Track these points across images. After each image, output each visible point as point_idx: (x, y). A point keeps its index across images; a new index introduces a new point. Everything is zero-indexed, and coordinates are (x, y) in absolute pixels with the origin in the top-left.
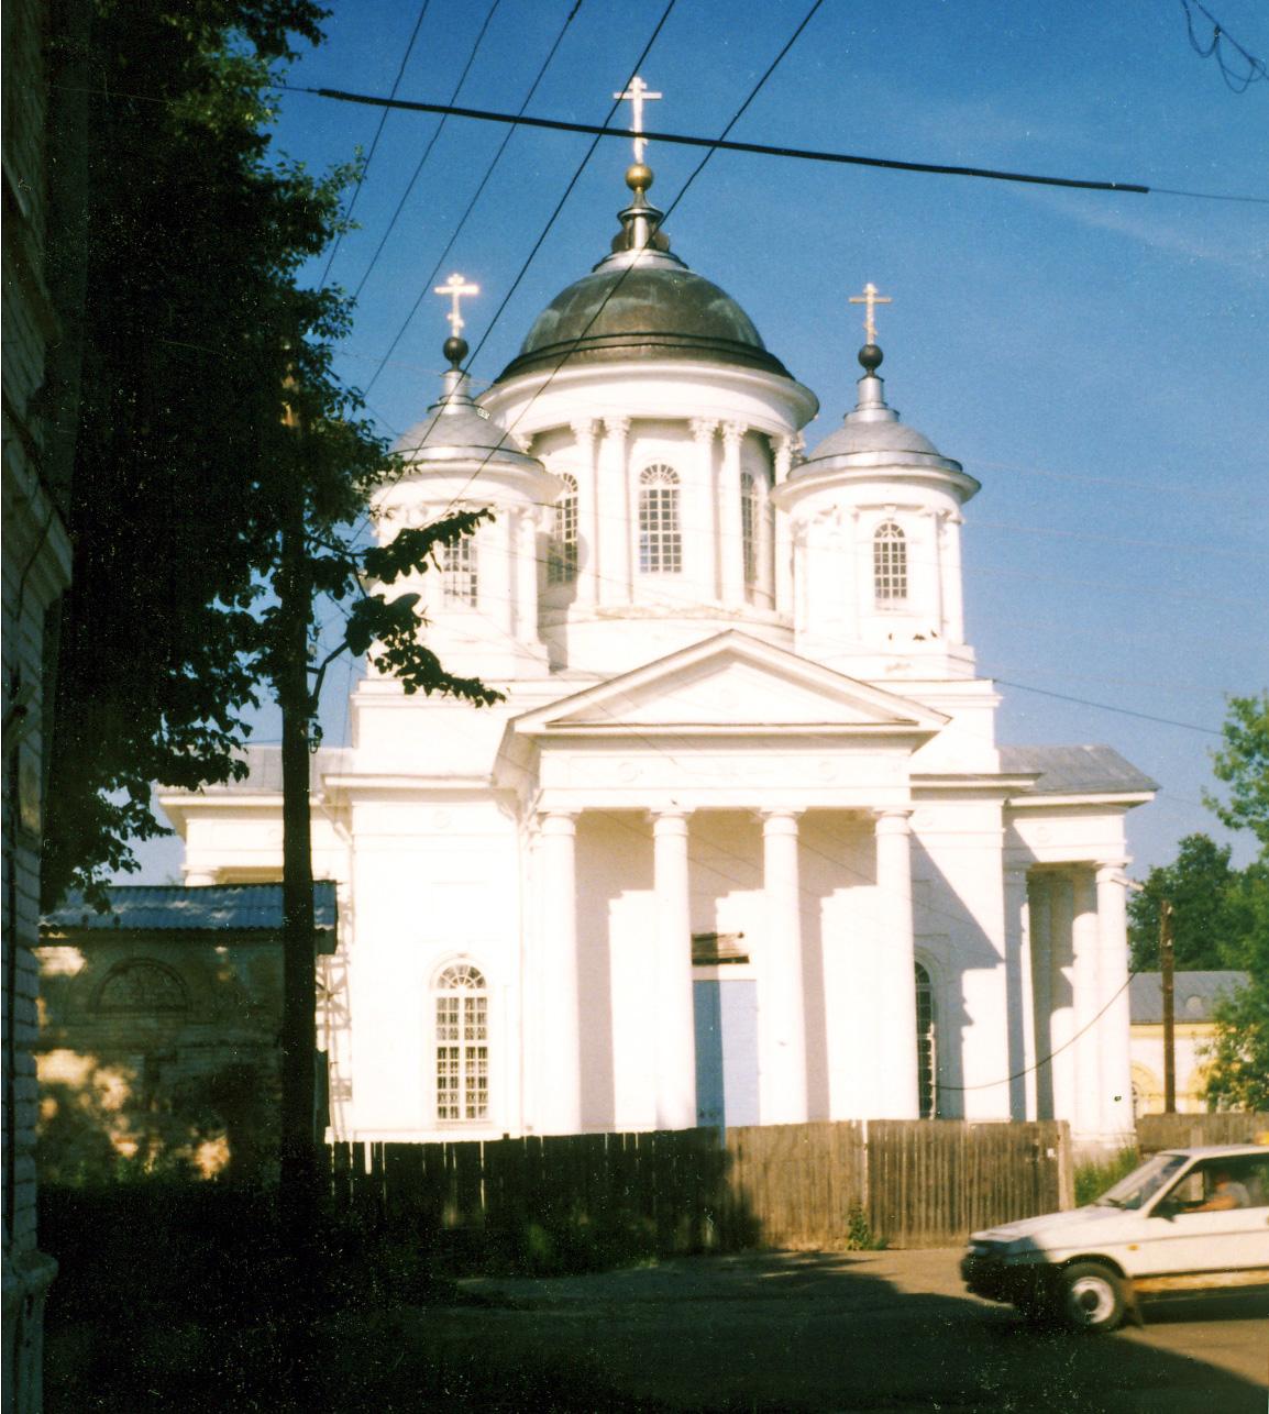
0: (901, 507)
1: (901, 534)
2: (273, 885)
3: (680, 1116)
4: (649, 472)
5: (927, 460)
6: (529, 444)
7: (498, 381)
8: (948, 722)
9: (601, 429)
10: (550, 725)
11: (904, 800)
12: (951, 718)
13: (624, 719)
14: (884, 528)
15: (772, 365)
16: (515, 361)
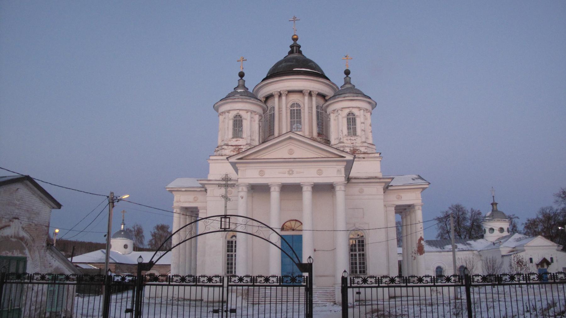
0: (353, 107)
1: (354, 115)
4: (293, 105)
5: (360, 95)
9: (280, 95)
14: (237, 116)
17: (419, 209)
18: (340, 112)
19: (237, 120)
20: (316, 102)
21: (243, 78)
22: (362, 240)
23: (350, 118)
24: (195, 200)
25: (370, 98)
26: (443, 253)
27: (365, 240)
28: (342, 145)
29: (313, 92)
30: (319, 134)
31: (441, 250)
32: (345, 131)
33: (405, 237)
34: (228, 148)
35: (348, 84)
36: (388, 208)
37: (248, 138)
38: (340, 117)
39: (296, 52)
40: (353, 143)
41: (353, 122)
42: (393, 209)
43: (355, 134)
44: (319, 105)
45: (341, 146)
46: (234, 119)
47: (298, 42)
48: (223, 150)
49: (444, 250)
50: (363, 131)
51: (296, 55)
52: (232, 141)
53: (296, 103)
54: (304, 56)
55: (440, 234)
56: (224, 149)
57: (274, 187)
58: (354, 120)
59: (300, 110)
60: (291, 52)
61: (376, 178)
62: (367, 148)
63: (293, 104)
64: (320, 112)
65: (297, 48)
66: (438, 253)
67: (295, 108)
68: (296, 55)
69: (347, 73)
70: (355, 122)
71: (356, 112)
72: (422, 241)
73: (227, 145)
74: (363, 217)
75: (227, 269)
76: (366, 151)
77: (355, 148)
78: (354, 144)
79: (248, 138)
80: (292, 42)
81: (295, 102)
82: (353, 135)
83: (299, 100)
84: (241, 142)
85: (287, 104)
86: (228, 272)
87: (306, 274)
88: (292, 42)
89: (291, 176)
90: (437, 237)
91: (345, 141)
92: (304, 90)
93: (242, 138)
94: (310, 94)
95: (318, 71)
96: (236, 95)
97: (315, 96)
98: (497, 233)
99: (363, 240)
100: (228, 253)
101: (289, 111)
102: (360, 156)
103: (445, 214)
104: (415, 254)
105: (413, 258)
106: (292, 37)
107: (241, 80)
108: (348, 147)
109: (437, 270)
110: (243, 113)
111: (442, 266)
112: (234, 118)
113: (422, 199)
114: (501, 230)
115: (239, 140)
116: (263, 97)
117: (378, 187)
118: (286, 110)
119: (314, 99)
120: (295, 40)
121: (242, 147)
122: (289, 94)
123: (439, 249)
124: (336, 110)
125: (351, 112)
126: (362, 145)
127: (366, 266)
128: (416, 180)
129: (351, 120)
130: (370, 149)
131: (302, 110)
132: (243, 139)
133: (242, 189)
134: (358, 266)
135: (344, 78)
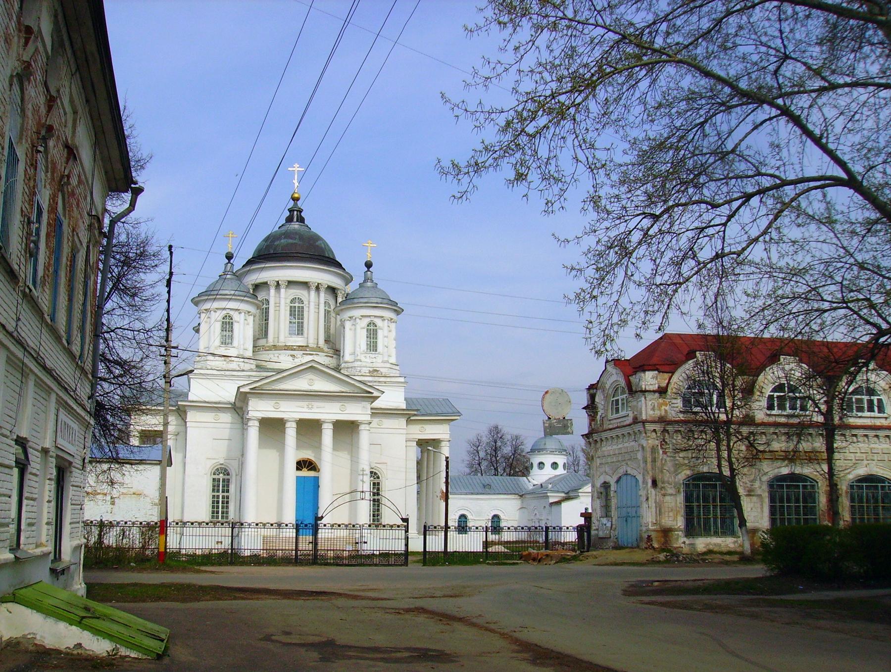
0: (375, 316)
1: (376, 326)
3: (441, 548)
4: (293, 301)
5: (385, 301)
9: (278, 285)
10: (251, 389)
11: (367, 418)
13: (278, 388)
14: (226, 316)
28: (359, 363)
30: (327, 341)
32: (364, 346)
38: (358, 327)
39: (297, 221)
58: (375, 332)
59: (303, 307)
60: (289, 220)
67: (297, 305)
68: (295, 226)
69: (369, 265)
89: (310, 411)
91: (363, 359)
94: (318, 288)
98: (548, 470)
100: (214, 494)
114: (555, 465)
119: (322, 294)
129: (372, 333)
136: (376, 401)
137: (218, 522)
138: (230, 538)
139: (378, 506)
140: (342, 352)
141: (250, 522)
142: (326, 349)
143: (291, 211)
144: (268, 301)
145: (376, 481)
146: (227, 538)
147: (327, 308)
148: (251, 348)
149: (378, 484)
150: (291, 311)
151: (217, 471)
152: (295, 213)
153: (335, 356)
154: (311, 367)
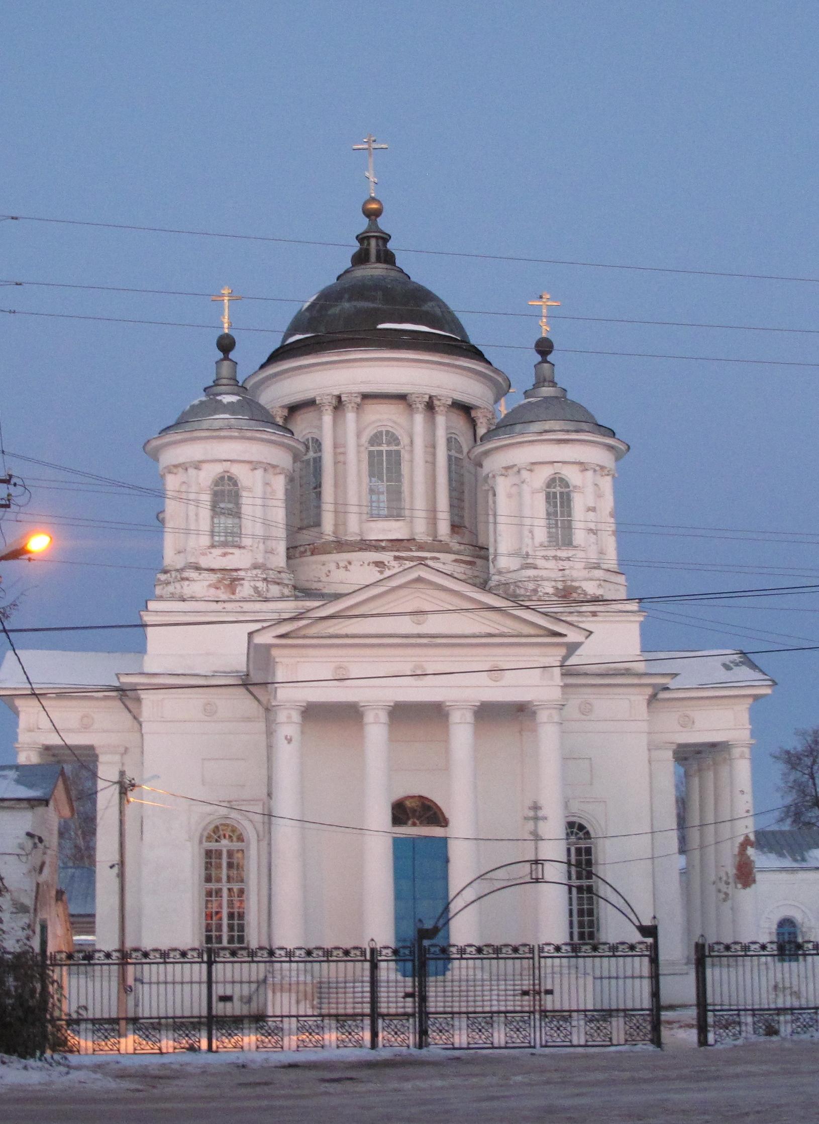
1: (567, 486)
2: (126, 1011)
4: (375, 439)
5: (584, 426)
6: (286, 412)
7: (263, 366)
8: (589, 635)
12: (591, 632)
14: (222, 478)
15: (476, 354)
16: (277, 350)
17: (742, 757)
18: (525, 474)
19: (223, 491)
20: (448, 428)
21: (232, 355)
22: (586, 848)
23: (555, 493)
24: (85, 727)
25: (612, 434)
26: (802, 875)
27: (596, 847)
28: (531, 573)
29: (439, 400)
30: (455, 527)
31: (795, 865)
32: (541, 535)
33: (713, 847)
34: (201, 577)
35: (546, 384)
36: (656, 754)
37: (257, 548)
39: (378, 260)
40: (564, 570)
41: (562, 506)
42: (669, 754)
43: (568, 542)
44: (453, 436)
45: (529, 577)
46: (216, 488)
47: (383, 223)
48: (187, 583)
49: (804, 865)
50: (591, 535)
51: (375, 270)
52: (210, 556)
53: (388, 432)
54: (402, 271)
55: (793, 808)
56: (187, 579)
57: (377, 711)
59: (398, 453)
60: (360, 258)
61: (627, 673)
62: (602, 583)
63: (376, 435)
64: (456, 458)
65: (381, 242)
66: (784, 876)
67: (384, 448)
69: (544, 348)
70: (569, 506)
71: (572, 475)
72: (749, 848)
73: (198, 568)
74: (591, 784)
75: (206, 931)
76: (599, 592)
77: (569, 583)
78: (567, 572)
79: (257, 548)
80: (363, 224)
81: (384, 429)
82: (564, 544)
83: (395, 422)
84: (238, 559)
85: (359, 435)
86: (209, 939)
87: (650, 940)
88: (363, 224)
90: (782, 820)
91: (540, 563)
92: (411, 394)
93: (240, 547)
94: (430, 406)
95: (451, 332)
96: (215, 414)
97: (444, 412)
99: (590, 848)
101: (365, 456)
102: (584, 609)
103: (809, 739)
104: (727, 883)
105: (722, 896)
106: (366, 203)
107: (226, 363)
108: (548, 579)
109: (782, 930)
110: (240, 472)
111: (798, 917)
112: (216, 486)
113: (750, 727)
115: (231, 553)
116: (283, 407)
117: (633, 698)
118: (359, 452)
119: (441, 420)
120: (372, 215)
121: (242, 574)
122: (366, 401)
123: (788, 863)
124: (515, 469)
125: (557, 476)
126: (587, 576)
127: (598, 919)
128: (736, 669)
130: (612, 586)
131: (403, 452)
132: (242, 551)
133: (289, 717)
134: (225, 922)
135: (535, 366)
136: (578, 652)
137: (224, 949)
138: (204, 987)
139: (590, 900)
140: (491, 550)
141: (290, 946)
142: (456, 547)
143: (362, 239)
144: (318, 444)
145: (583, 845)
146: (196, 986)
147: (453, 453)
148: (281, 548)
149: (588, 851)
150: (371, 464)
151: (216, 832)
152: (373, 242)
153: (478, 561)
154: (419, 580)
